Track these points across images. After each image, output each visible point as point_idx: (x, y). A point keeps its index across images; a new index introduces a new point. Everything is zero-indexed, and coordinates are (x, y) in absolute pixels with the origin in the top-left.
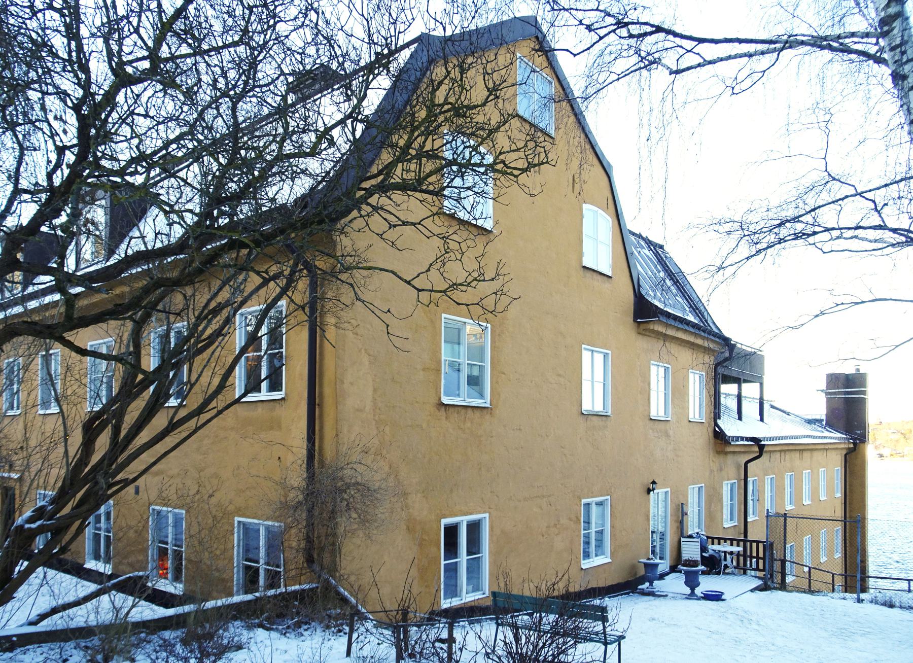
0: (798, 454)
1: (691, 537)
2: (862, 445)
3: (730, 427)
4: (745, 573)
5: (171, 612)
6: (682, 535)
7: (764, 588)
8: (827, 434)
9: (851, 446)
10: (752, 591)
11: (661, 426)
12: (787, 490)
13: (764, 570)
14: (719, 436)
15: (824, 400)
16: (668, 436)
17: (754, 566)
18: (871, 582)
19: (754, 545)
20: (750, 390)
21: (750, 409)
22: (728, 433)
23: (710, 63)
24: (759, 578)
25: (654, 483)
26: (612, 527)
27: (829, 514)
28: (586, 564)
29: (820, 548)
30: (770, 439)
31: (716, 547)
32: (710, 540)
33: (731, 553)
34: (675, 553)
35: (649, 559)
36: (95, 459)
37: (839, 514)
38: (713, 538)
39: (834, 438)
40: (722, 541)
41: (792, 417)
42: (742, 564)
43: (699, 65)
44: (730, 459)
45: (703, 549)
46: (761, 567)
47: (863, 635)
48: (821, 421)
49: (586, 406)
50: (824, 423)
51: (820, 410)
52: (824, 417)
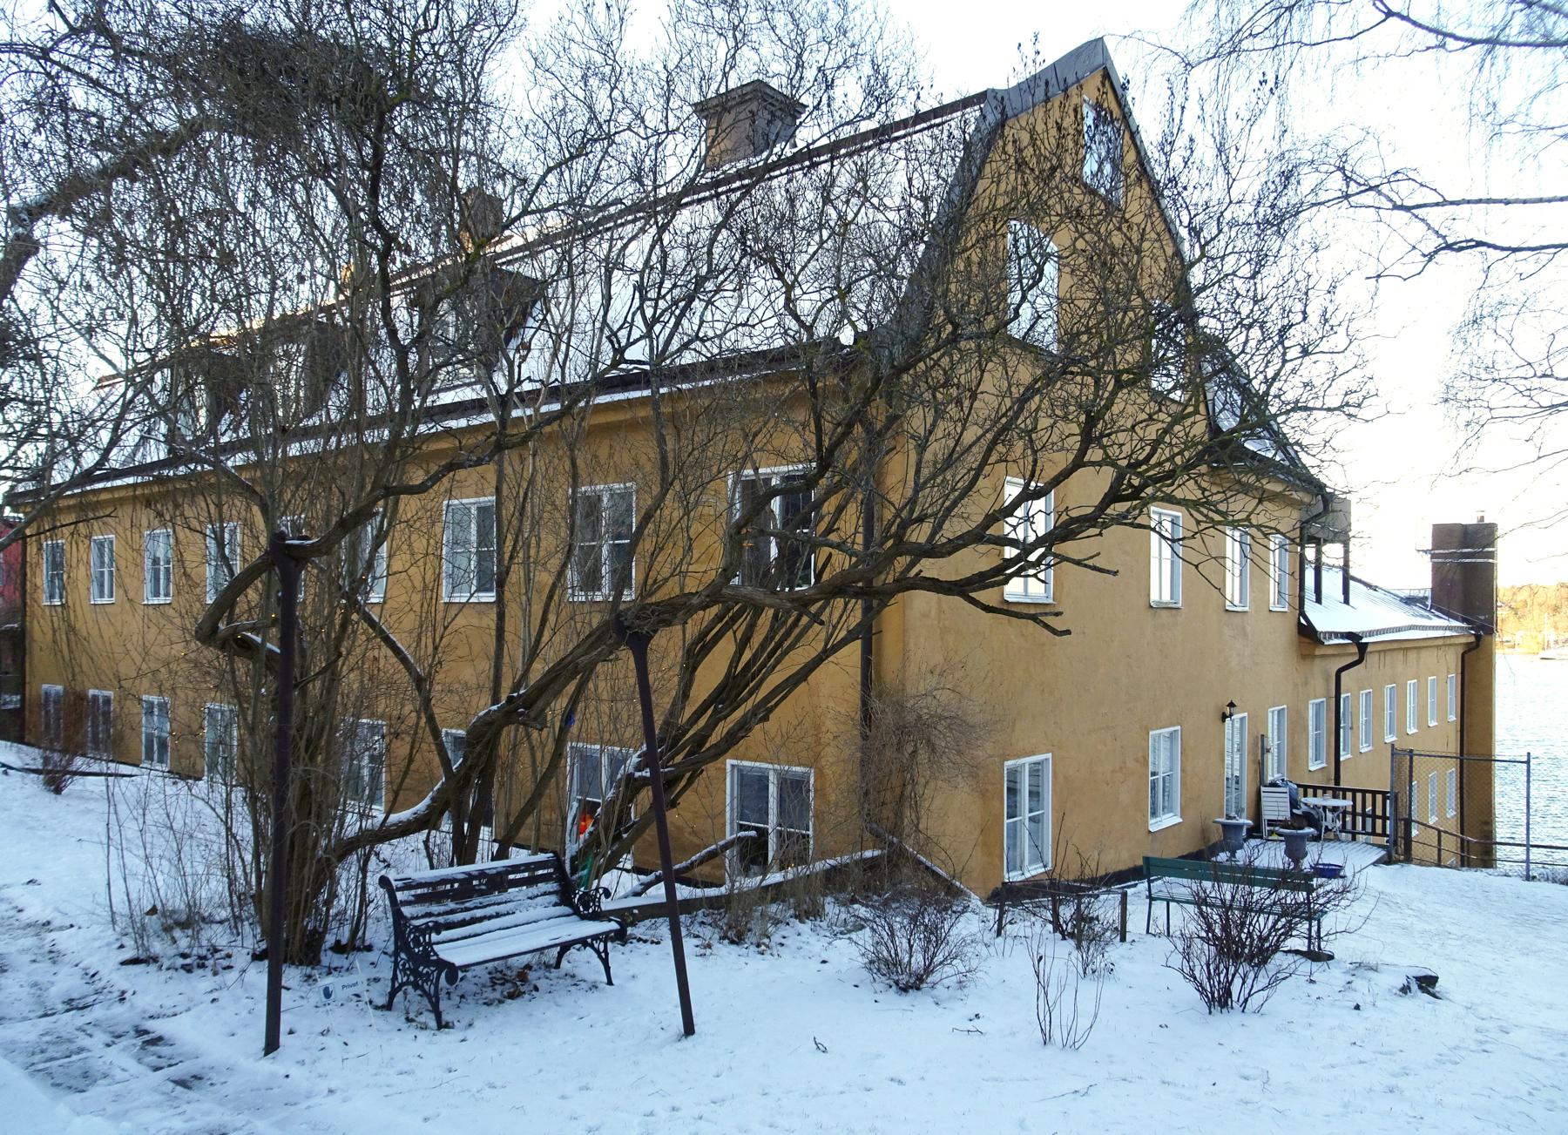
0: (1400, 656)
1: (1274, 785)
2: (1487, 638)
3: (1324, 618)
4: (1354, 839)
5: (698, 893)
6: (1262, 782)
7: (1388, 861)
8: (1436, 622)
9: (1472, 639)
10: (1375, 864)
11: (1237, 620)
12: (1387, 712)
13: (1384, 834)
14: (1307, 632)
15: (1430, 565)
16: (1245, 634)
17: (1369, 829)
18: (1501, 852)
19: (1369, 796)
20: (1332, 552)
21: (1332, 582)
22: (1319, 628)
23: (1452, 203)
24: (1380, 846)
25: (1231, 705)
26: (1183, 770)
27: (1439, 748)
28: (1156, 825)
29: (1435, 804)
30: (1371, 633)
31: (1311, 800)
32: (1301, 790)
33: (1334, 809)
34: (1253, 809)
35: (1229, 817)
36: (575, 682)
37: (1454, 748)
38: (1306, 787)
39: (1446, 628)
40: (1320, 792)
41: (1379, 594)
42: (1349, 827)
43: (1437, 204)
44: (1318, 665)
45: (1294, 804)
46: (1379, 830)
47: (1554, 923)
48: (1422, 600)
49: (1154, 597)
50: (1429, 603)
51: (1421, 579)
52: (1428, 594)
